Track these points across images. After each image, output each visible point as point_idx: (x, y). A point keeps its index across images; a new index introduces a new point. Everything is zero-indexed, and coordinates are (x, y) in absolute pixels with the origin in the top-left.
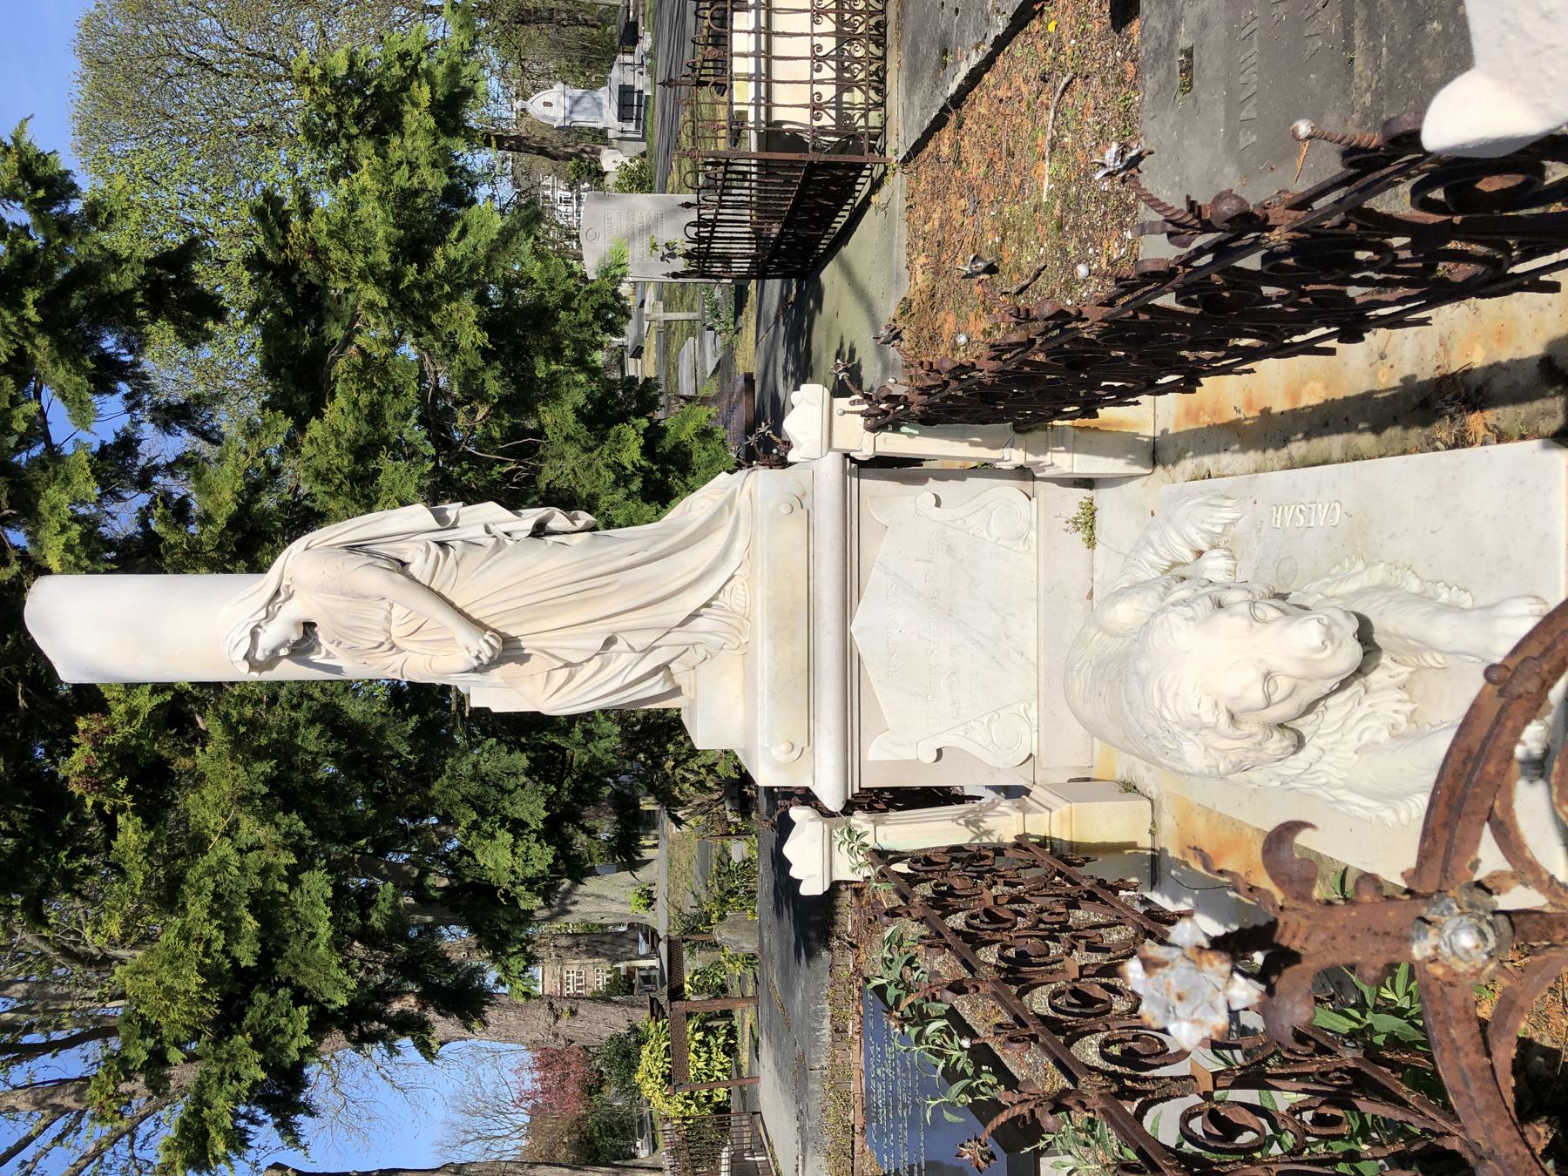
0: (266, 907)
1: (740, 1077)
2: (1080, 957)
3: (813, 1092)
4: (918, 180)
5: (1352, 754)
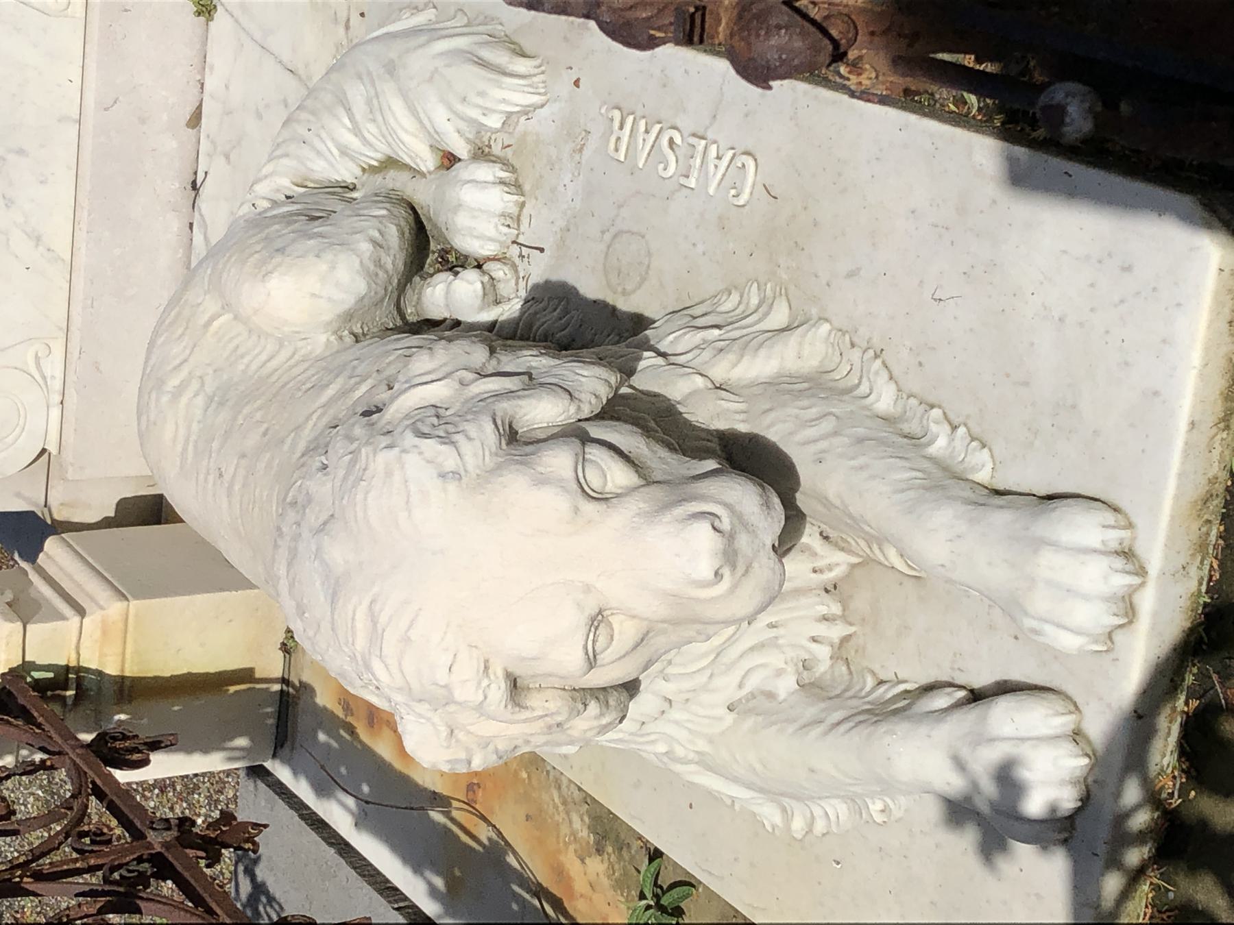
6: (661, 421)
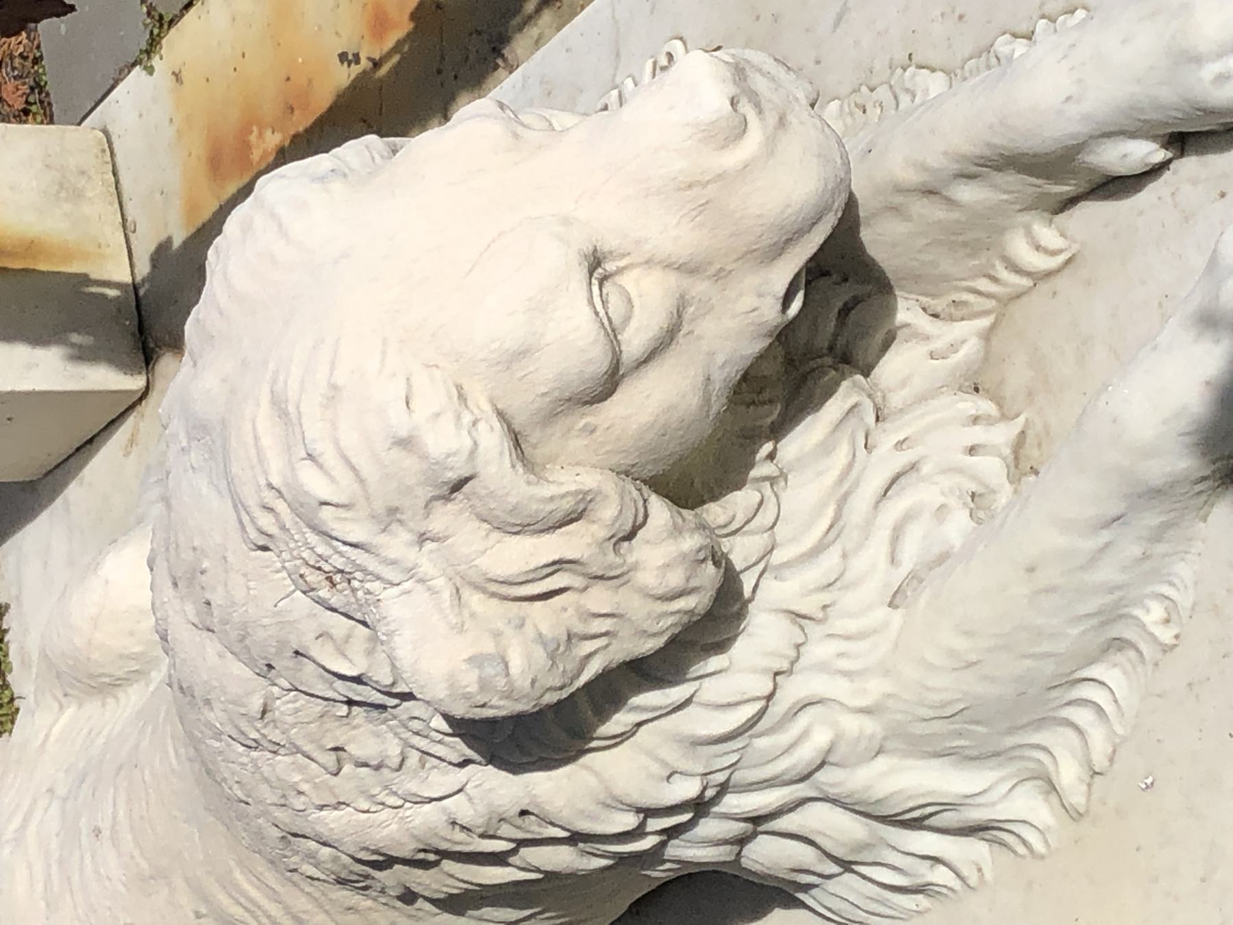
5: (882, 612)
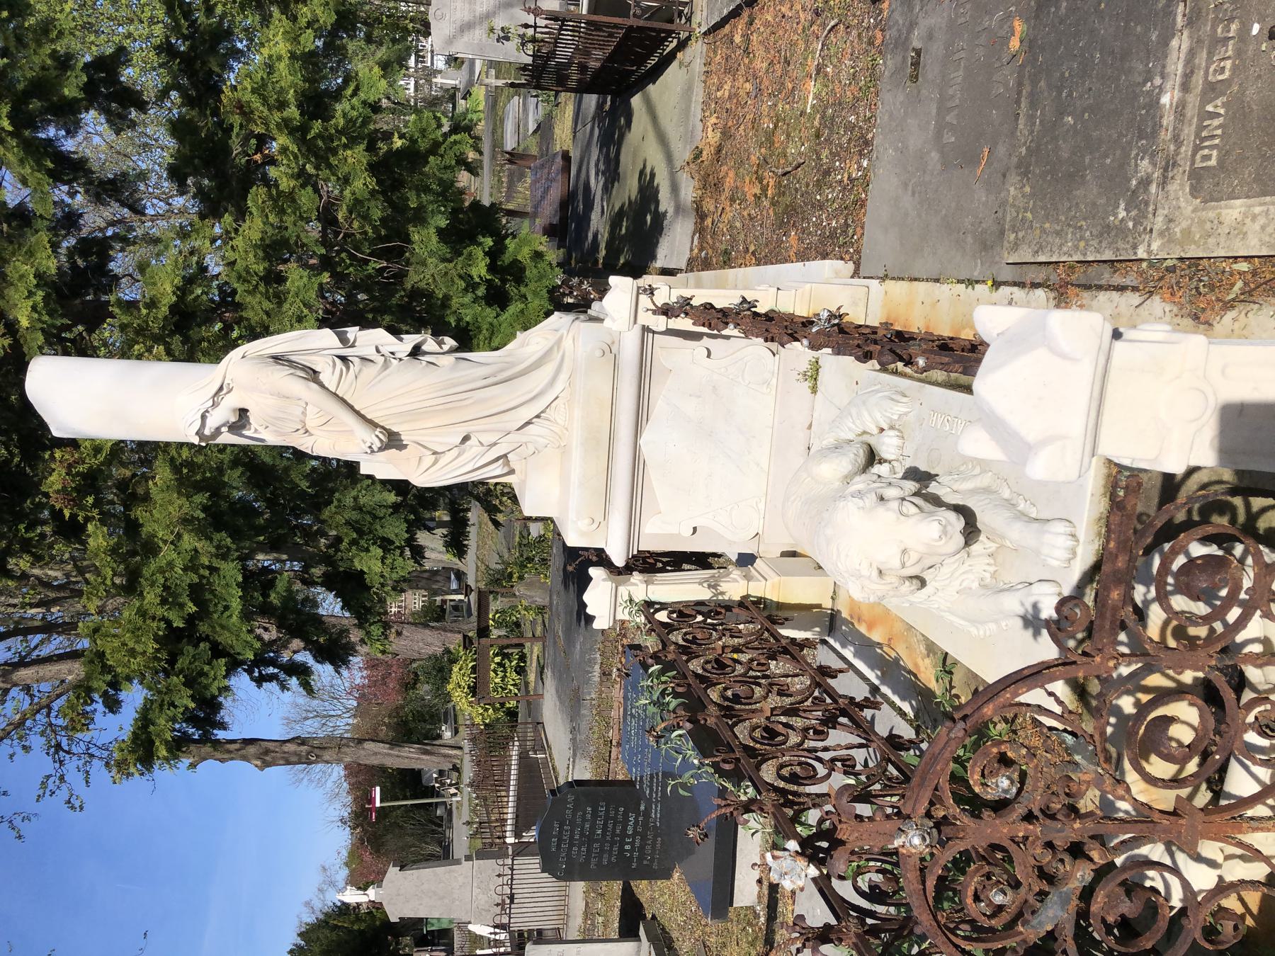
0: (196, 592)
1: (527, 692)
2: (774, 700)
3: (584, 716)
4: (715, 52)
6: (936, 501)
